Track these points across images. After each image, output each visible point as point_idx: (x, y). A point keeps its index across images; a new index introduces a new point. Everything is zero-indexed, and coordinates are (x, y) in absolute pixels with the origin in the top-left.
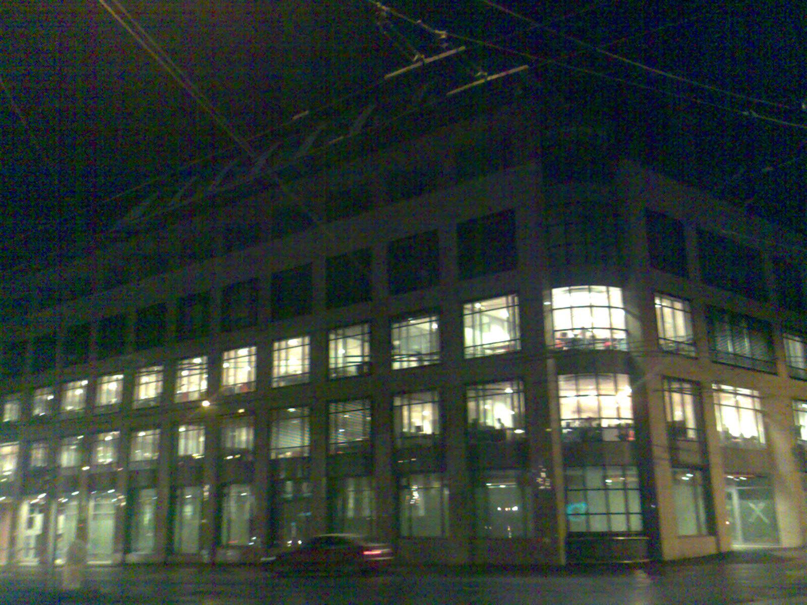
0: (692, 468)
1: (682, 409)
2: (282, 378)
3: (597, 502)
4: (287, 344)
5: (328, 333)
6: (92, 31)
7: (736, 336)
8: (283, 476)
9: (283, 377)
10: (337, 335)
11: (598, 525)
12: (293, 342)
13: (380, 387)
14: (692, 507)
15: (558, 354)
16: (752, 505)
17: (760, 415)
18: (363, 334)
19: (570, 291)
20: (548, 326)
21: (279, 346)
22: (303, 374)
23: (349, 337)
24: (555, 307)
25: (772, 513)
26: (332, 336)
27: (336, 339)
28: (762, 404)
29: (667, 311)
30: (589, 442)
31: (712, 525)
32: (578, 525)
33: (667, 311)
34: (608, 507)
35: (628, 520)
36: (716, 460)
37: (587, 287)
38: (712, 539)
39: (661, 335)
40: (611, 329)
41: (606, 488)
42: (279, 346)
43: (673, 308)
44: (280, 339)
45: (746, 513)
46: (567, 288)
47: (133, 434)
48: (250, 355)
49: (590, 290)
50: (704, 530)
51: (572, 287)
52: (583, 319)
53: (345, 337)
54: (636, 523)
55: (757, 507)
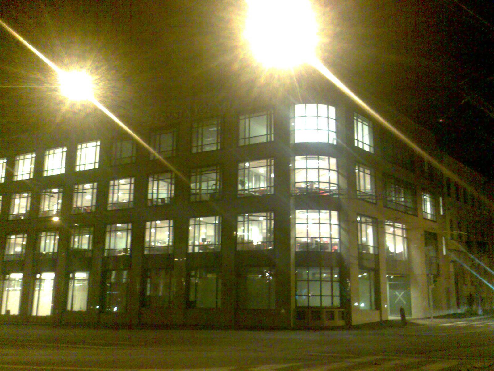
0: (369, 270)
1: (368, 236)
2: (114, 204)
3: (315, 289)
4: (119, 183)
5: (148, 176)
6: (444, 60)
7: (397, 192)
8: (111, 267)
9: (115, 203)
10: (153, 178)
11: (315, 302)
12: (122, 181)
13: (180, 212)
14: (124, 240)
15: (297, 197)
16: (397, 293)
17: (405, 240)
18: (171, 179)
19: (306, 158)
20: (292, 181)
21: (114, 183)
22: (129, 202)
23: (160, 180)
24: (296, 168)
25: (408, 297)
26: (150, 179)
27: (153, 181)
28: (407, 233)
29: (361, 174)
30: (314, 255)
31: (377, 304)
32: (303, 301)
33: (361, 174)
34: (317, 292)
35: (332, 299)
36: (383, 267)
37: (317, 156)
38: (378, 312)
39: (358, 189)
40: (330, 183)
41: (321, 280)
42: (114, 183)
43: (364, 172)
44: (114, 179)
45: (393, 297)
46: (305, 156)
47: (9, 237)
48: (93, 188)
49: (318, 159)
50: (374, 308)
51: (308, 156)
52: (313, 176)
53: (158, 180)
54: (337, 302)
55: (400, 295)
